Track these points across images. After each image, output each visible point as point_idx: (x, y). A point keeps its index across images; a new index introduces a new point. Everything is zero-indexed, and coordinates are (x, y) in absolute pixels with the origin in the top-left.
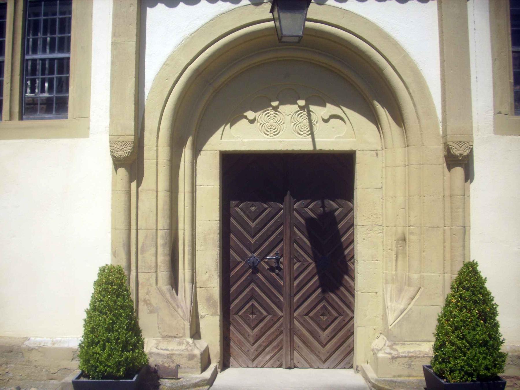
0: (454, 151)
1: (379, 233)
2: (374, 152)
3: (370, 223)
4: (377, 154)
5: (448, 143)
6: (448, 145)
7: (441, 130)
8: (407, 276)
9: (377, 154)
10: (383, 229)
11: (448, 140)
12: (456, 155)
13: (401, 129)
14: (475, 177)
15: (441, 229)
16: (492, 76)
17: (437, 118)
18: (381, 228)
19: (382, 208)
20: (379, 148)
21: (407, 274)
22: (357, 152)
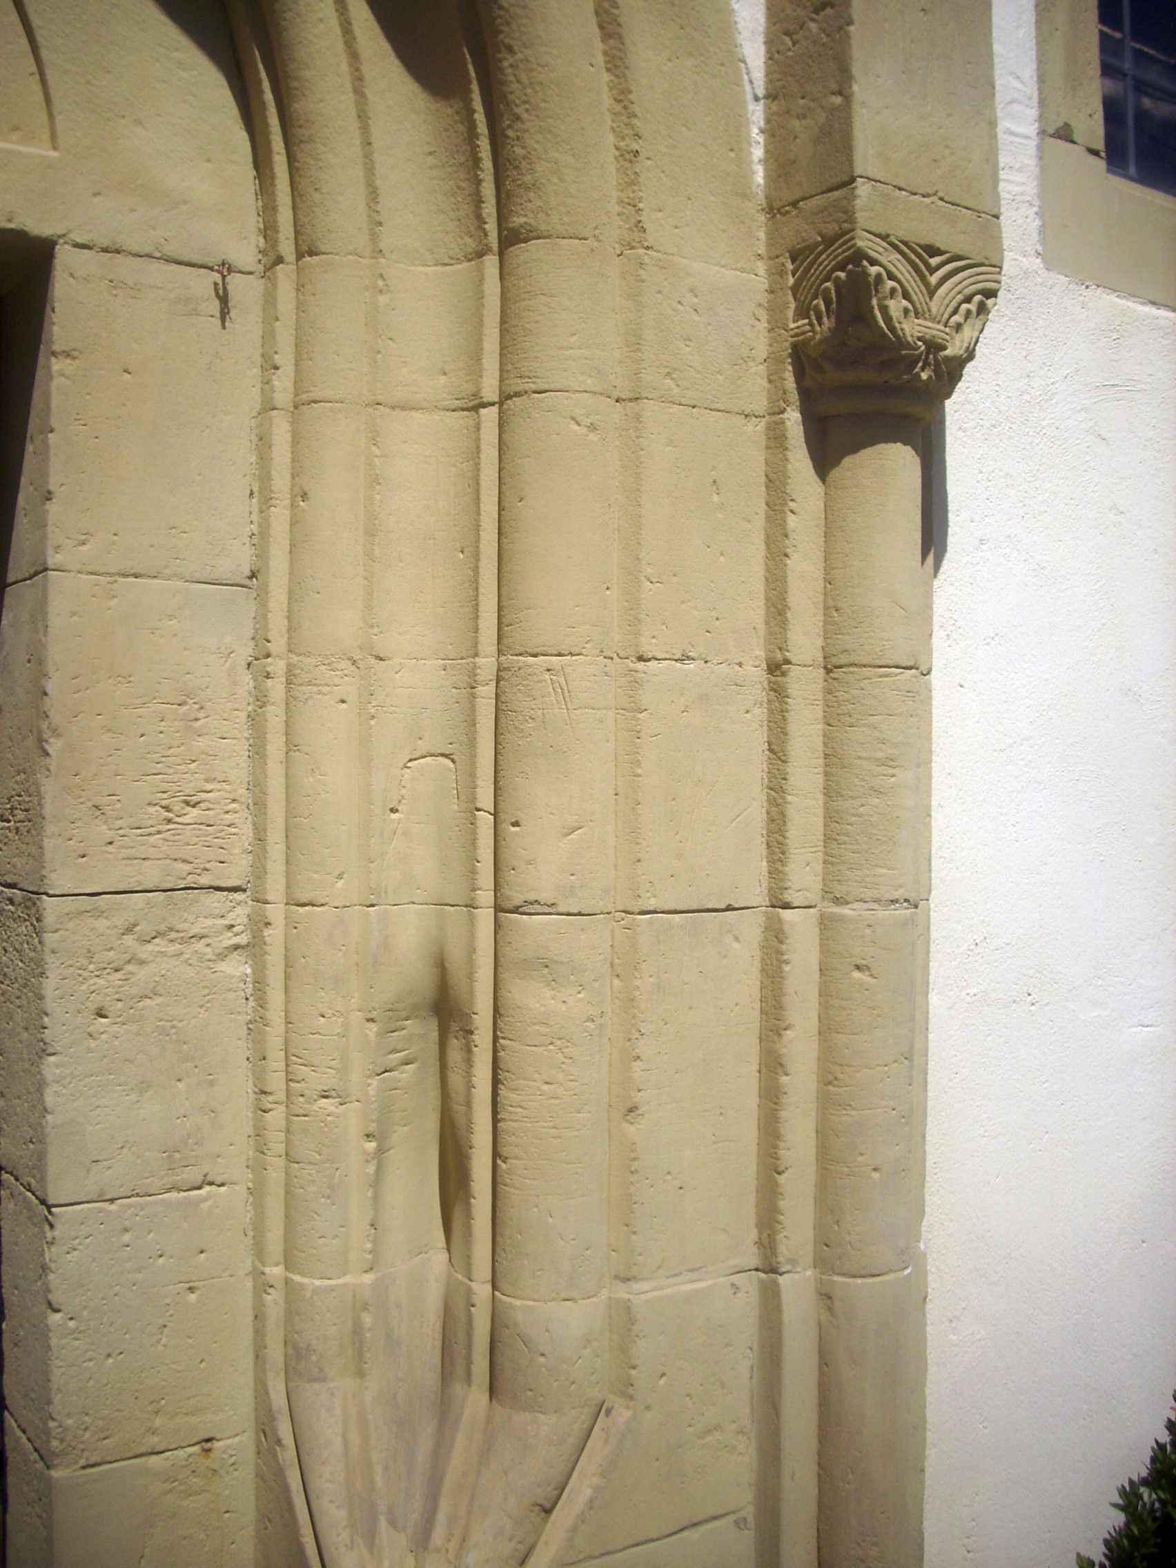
0: (896, 306)
1: (222, 957)
2: (203, 283)
3: (151, 875)
4: (224, 299)
5: (863, 242)
6: (859, 256)
7: (758, 153)
8: (274, 1299)
9: (224, 299)
10: (259, 923)
11: (862, 218)
12: (901, 343)
13: (447, 111)
14: (952, 540)
15: (751, 927)
16: (14, 533)
17: (735, 60)
18: (240, 915)
19: (258, 751)
20: (245, 253)
21: (275, 1272)
22: (64, 257)
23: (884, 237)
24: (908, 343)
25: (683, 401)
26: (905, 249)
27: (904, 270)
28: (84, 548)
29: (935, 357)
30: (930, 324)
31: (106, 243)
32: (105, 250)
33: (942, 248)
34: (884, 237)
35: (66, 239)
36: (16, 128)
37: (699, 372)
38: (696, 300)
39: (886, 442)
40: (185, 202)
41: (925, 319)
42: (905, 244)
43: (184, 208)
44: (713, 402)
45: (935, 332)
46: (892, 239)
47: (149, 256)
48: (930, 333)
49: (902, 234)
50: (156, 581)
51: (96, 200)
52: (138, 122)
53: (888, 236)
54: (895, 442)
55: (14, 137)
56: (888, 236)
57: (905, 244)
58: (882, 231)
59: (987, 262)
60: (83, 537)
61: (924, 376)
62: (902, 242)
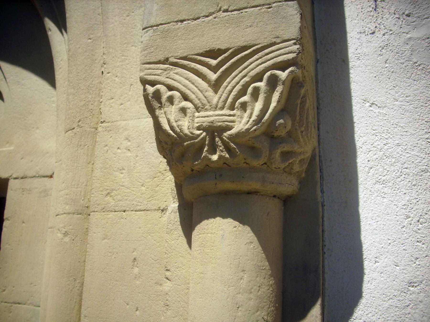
22: (12, 184)
23: (166, 61)
24: (186, 135)
25: (117, 209)
26: (186, 62)
27: (237, 79)
28: (4, 293)
29: (222, 140)
30: (211, 113)
31: (22, 175)
32: (22, 178)
33: (223, 48)
34: (166, 61)
35: (12, 177)
36: (8, 142)
37: (128, 188)
38: (129, 144)
39: (208, 219)
40: (48, 153)
41: (206, 110)
42: (185, 58)
43: (48, 155)
44: (137, 205)
45: (212, 119)
46: (172, 60)
47: (34, 177)
48: (206, 122)
49: (180, 53)
50: (25, 306)
51: (22, 160)
52: (37, 128)
53: (167, 59)
54: (214, 217)
55: (8, 145)
56: (167, 59)
57: (185, 58)
58: (161, 57)
59: (278, 40)
60: (4, 288)
61: (215, 157)
62: (181, 58)
